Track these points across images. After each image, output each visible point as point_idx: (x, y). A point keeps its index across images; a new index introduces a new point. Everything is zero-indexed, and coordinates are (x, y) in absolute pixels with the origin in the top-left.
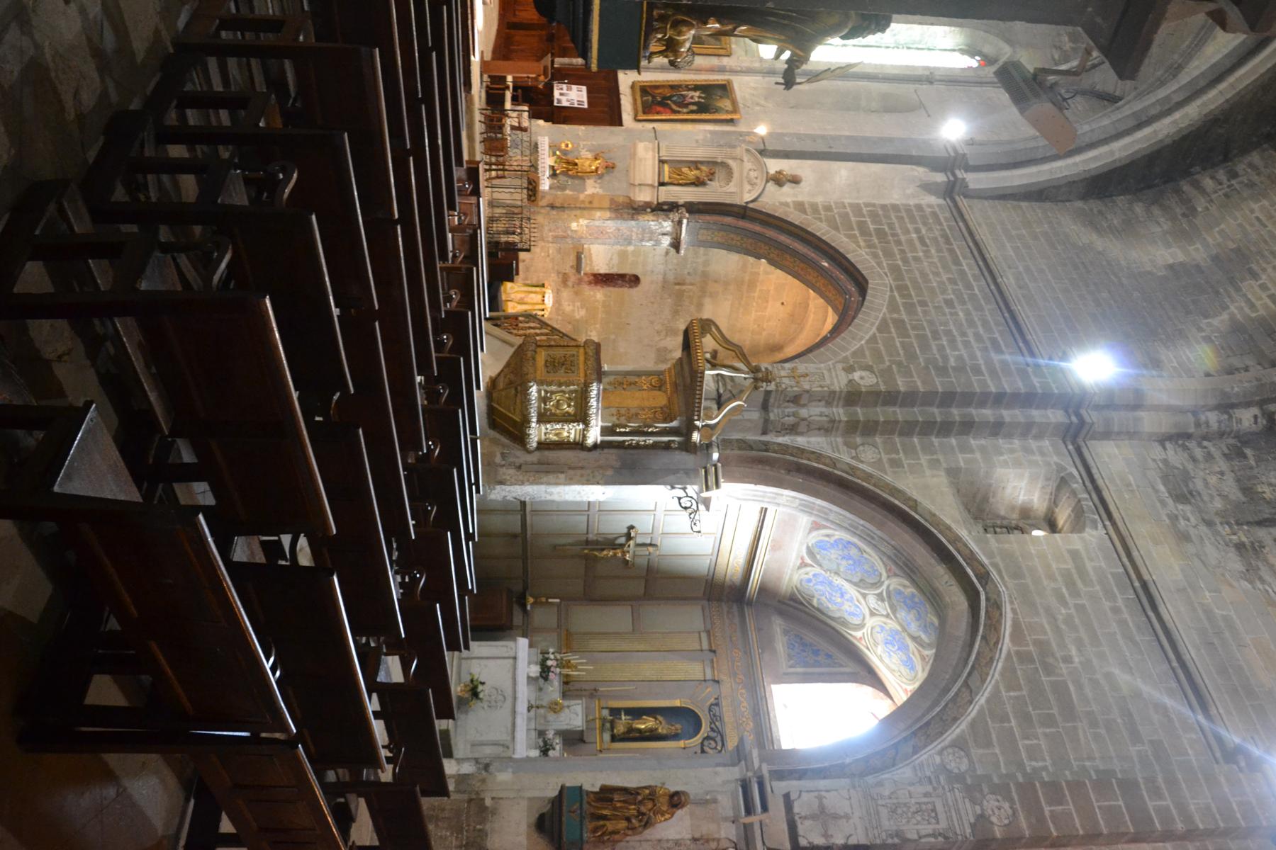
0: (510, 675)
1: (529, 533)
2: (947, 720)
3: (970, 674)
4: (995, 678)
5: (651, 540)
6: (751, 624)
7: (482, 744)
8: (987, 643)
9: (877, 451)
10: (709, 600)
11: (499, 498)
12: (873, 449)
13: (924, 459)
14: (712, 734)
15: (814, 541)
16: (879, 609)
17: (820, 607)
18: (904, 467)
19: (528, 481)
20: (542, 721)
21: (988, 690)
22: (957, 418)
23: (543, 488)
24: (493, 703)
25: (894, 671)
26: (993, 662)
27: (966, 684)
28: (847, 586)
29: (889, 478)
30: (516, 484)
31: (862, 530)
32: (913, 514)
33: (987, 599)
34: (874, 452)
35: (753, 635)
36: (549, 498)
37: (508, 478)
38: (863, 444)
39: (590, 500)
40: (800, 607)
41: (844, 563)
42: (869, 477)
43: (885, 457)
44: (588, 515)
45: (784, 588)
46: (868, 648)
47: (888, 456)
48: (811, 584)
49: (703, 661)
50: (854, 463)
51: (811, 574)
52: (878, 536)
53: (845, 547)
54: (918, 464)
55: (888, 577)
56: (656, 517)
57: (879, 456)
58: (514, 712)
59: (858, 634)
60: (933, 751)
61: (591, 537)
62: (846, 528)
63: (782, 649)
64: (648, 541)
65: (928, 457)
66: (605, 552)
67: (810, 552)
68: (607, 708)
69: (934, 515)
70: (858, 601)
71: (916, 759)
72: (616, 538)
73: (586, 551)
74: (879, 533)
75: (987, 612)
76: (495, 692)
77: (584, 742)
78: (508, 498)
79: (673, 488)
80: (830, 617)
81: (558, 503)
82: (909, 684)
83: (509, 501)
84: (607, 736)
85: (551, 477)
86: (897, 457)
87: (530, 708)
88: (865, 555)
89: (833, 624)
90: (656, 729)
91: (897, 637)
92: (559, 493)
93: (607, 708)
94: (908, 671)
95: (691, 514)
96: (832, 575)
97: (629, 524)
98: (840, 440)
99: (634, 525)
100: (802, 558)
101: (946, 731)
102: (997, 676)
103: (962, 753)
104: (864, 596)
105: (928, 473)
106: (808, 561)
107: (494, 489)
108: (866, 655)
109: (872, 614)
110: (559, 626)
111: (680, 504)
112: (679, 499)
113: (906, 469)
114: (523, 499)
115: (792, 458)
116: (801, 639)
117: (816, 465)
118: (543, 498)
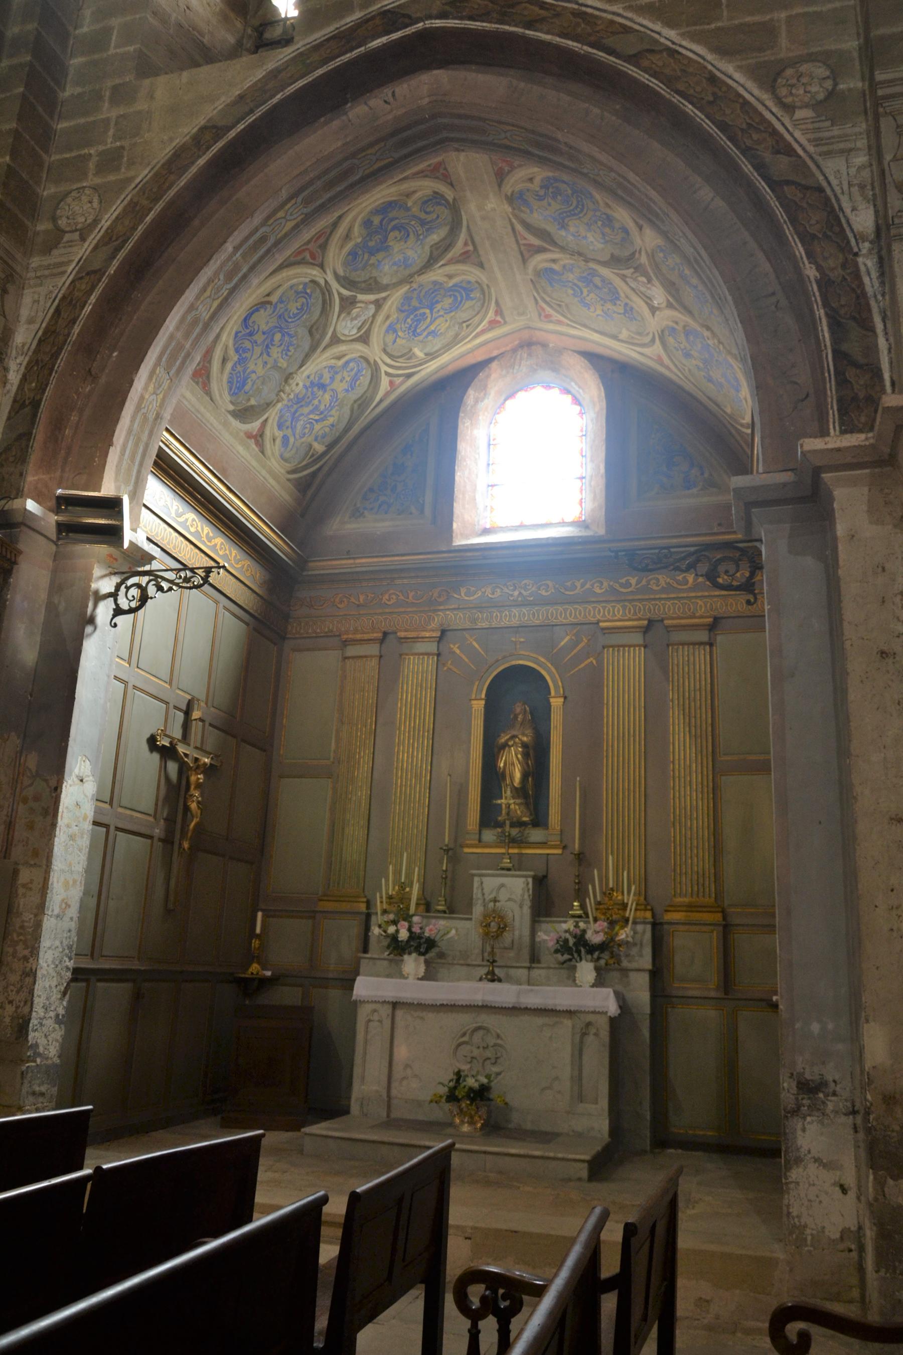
0: (430, 1016)
1: (136, 965)
2: (714, 94)
3: (611, 52)
4: (621, 11)
5: (180, 710)
6: (344, 565)
7: (578, 1079)
8: (543, 20)
9: (74, 194)
10: (284, 638)
11: (58, 1034)
12: (69, 200)
13: (109, 112)
14: (703, 568)
15: (227, 398)
16: (363, 318)
17: (328, 440)
18: (122, 147)
19: (26, 959)
20: (512, 954)
21: (645, 22)
22: (31, 26)
23: (49, 924)
24: (489, 1053)
25: (457, 335)
26: (585, 13)
27: (634, 59)
28: (310, 369)
29: (143, 174)
30: (31, 992)
31: (244, 256)
32: (232, 134)
33: (443, 15)
34: (78, 199)
35: (364, 562)
36: (73, 911)
37: (10, 1009)
38: (54, 219)
39: (91, 815)
40: (320, 476)
41: (275, 352)
42: (134, 211)
43: (93, 180)
44: (118, 829)
45: (287, 497)
46: (409, 376)
47: (90, 176)
48: (292, 440)
49: (401, 655)
50: (94, 237)
51: (279, 434)
52: (264, 223)
53: (251, 334)
54: (116, 124)
55: (322, 266)
56: (138, 685)
57: (87, 191)
58: (515, 1010)
59: (385, 384)
60: (787, 121)
61: (157, 832)
62: (232, 291)
63: (387, 524)
64: (180, 716)
65: (106, 105)
66: (193, 806)
67: (243, 414)
68: (480, 834)
69: (241, 97)
70: (339, 358)
71: (804, 149)
72: (167, 778)
73: (186, 845)
74: (257, 219)
75: (471, 18)
76: (464, 1050)
77: (545, 877)
78: (61, 1011)
79: (91, 621)
80: (346, 430)
81: (86, 893)
82: (487, 312)
83: (67, 1009)
84: (536, 835)
85: (25, 902)
86: (95, 159)
87: (493, 978)
88: (274, 298)
89: (356, 429)
90: (525, 746)
91: (415, 303)
92: (66, 885)
93: (480, 834)
94: (469, 304)
95: (160, 589)
96: (287, 388)
97: (145, 747)
98: (35, 261)
99: (148, 736)
100: (249, 436)
101: (740, 96)
102: (614, 8)
103: (789, 72)
104: (336, 340)
105: (141, 105)
106: (255, 426)
107: (36, 1045)
108: (416, 385)
109: (364, 339)
110: (312, 915)
111: (131, 611)
112: (118, 611)
113: (126, 143)
114: (69, 975)
115: (64, 355)
116: (371, 490)
117: (88, 308)
118: (73, 925)
